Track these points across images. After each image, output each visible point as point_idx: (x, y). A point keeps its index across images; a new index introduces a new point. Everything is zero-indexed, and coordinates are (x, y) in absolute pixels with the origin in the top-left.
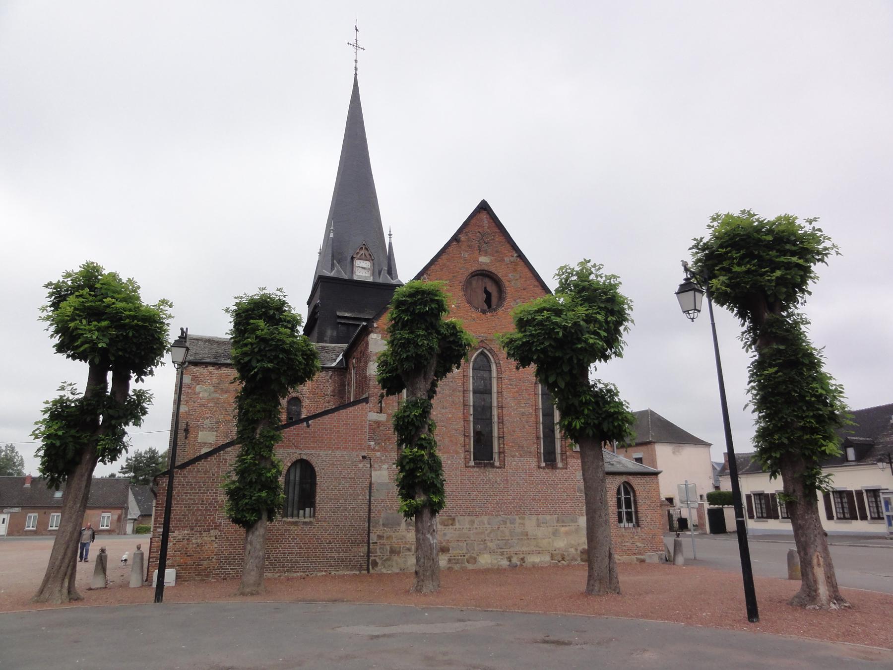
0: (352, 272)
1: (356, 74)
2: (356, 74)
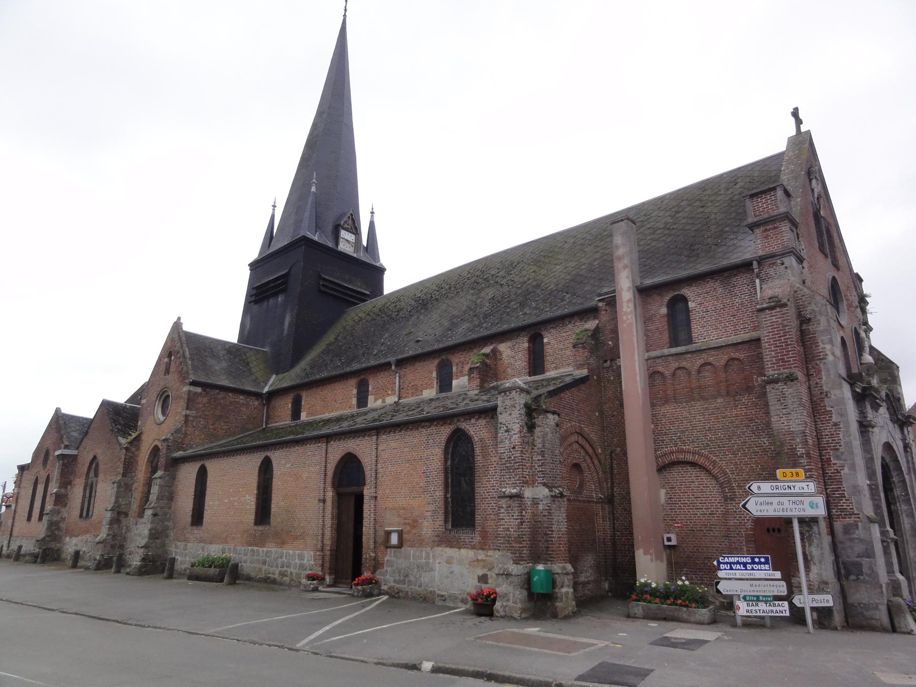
0: (337, 244)
1: (345, 15)
2: (345, 15)
